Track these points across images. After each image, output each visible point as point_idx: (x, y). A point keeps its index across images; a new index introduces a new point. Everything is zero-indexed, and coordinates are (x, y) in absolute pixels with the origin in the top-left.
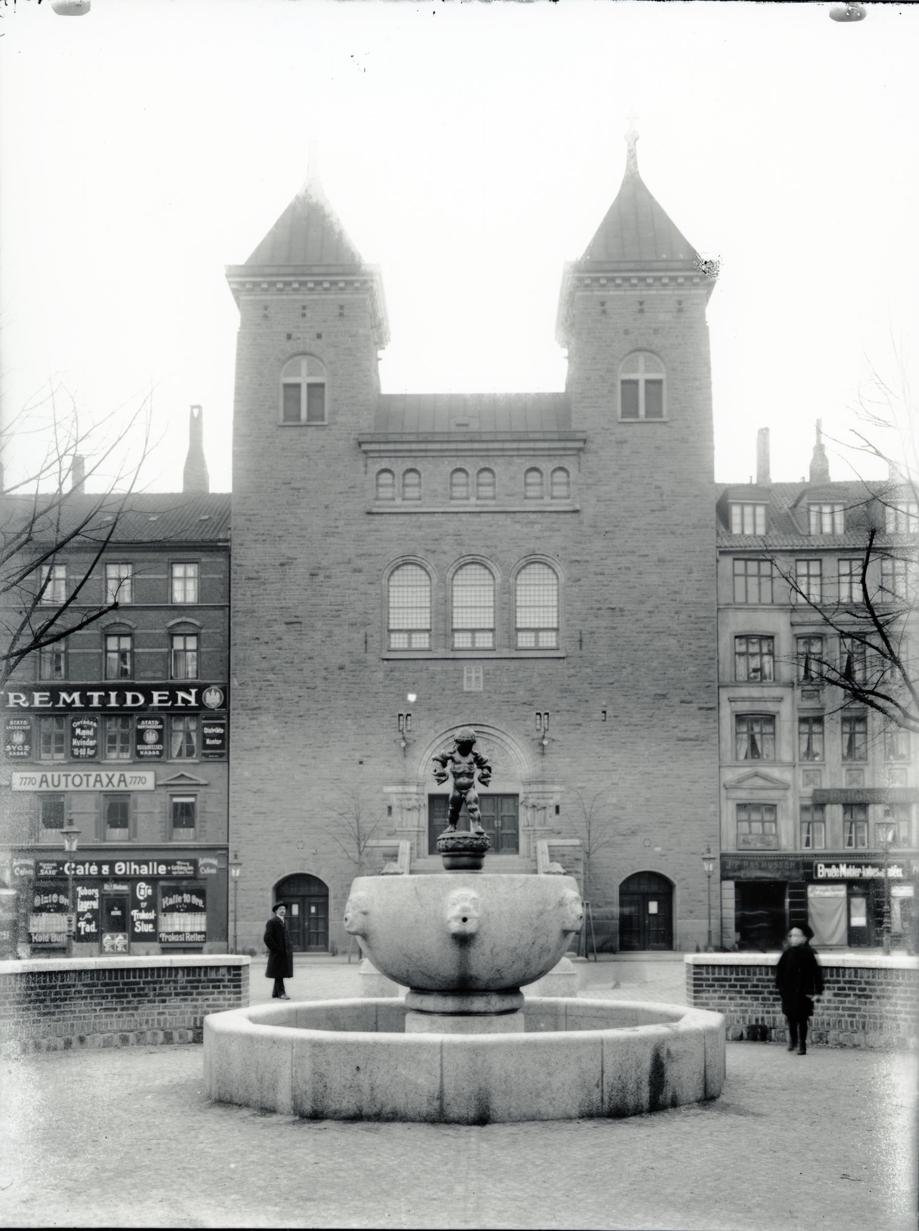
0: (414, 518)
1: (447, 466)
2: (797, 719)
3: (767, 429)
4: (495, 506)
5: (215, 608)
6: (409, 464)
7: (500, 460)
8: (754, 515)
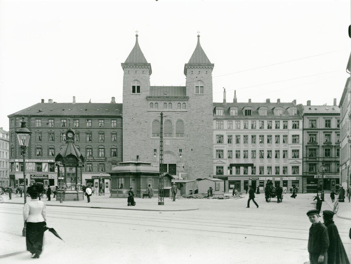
0: (157, 112)
1: (163, 102)
2: (235, 151)
3: (251, 99)
4: (157, 110)
5: (119, 129)
6: (156, 102)
7: (173, 101)
8: (218, 113)
